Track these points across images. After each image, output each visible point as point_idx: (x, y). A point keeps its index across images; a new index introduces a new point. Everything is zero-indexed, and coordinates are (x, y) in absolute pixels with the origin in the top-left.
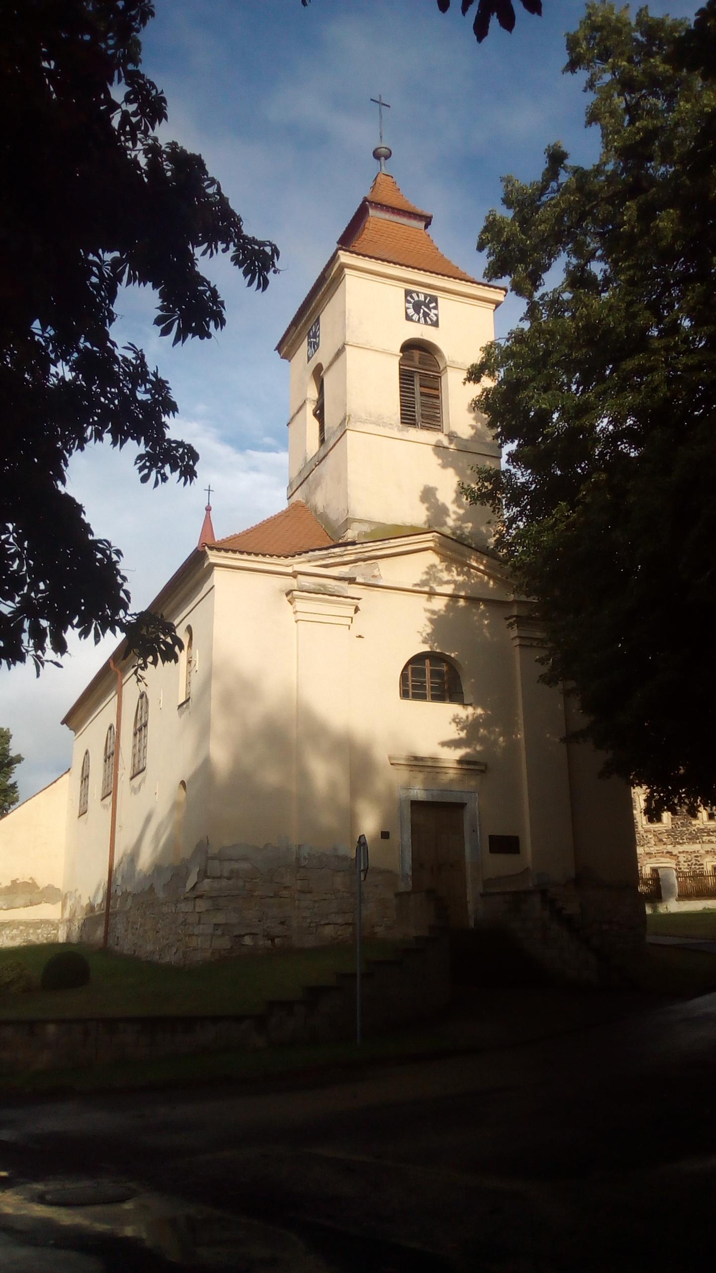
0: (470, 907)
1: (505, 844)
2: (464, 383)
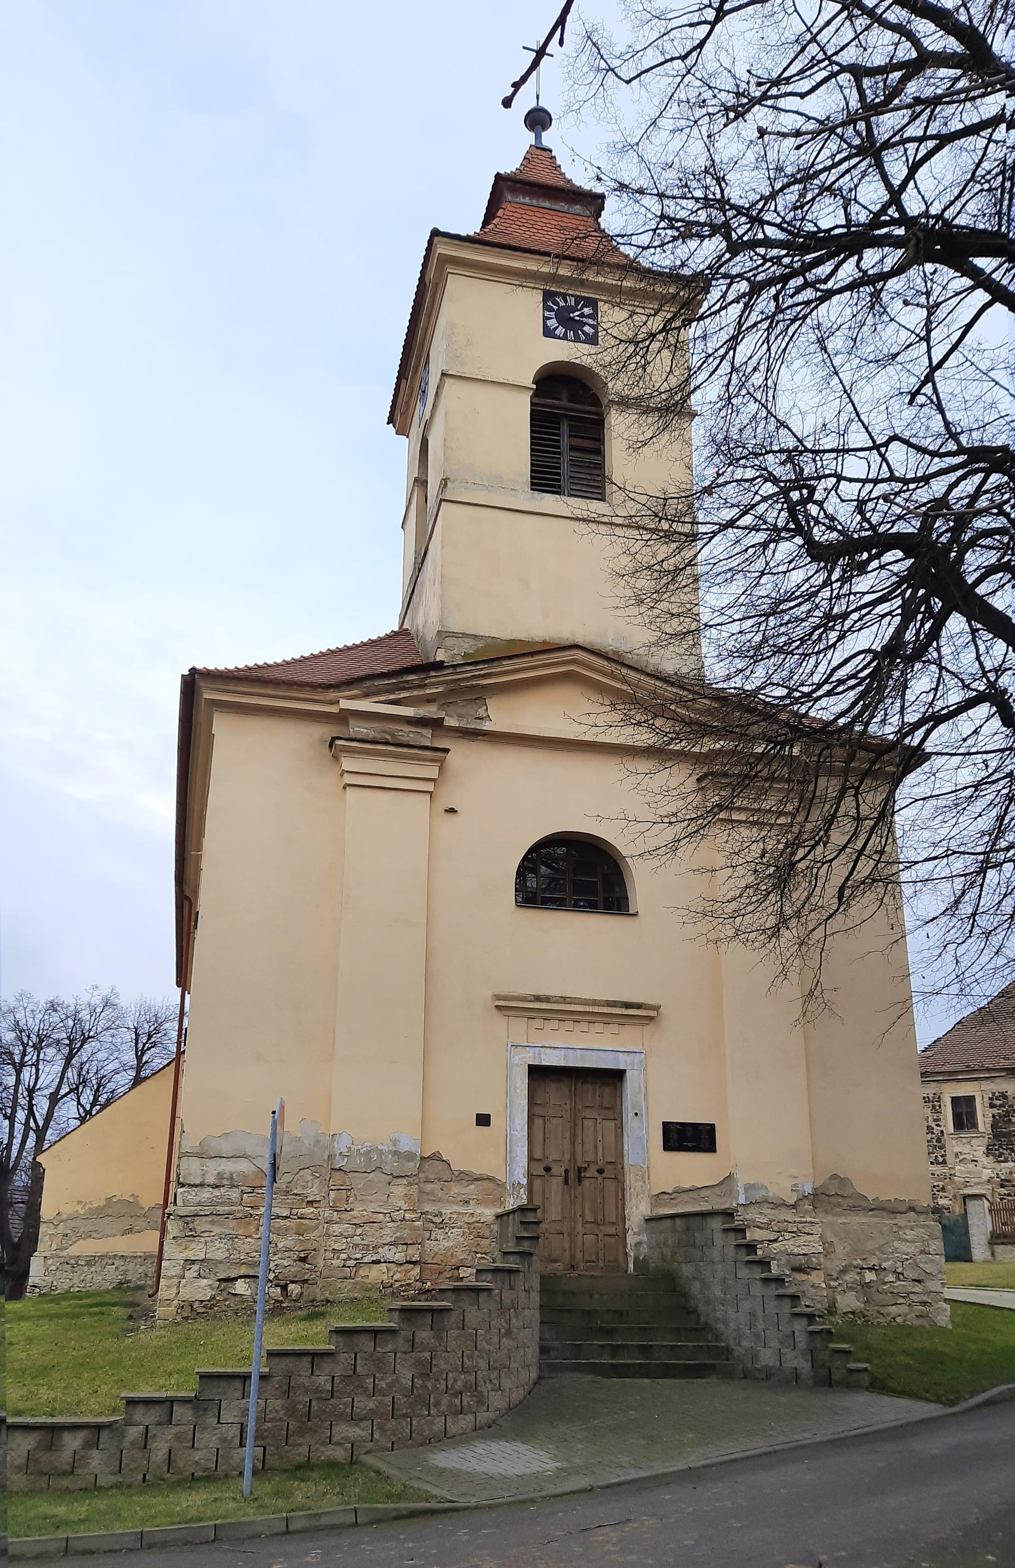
0: (631, 1240)
1: (689, 1137)
2: (635, 915)
